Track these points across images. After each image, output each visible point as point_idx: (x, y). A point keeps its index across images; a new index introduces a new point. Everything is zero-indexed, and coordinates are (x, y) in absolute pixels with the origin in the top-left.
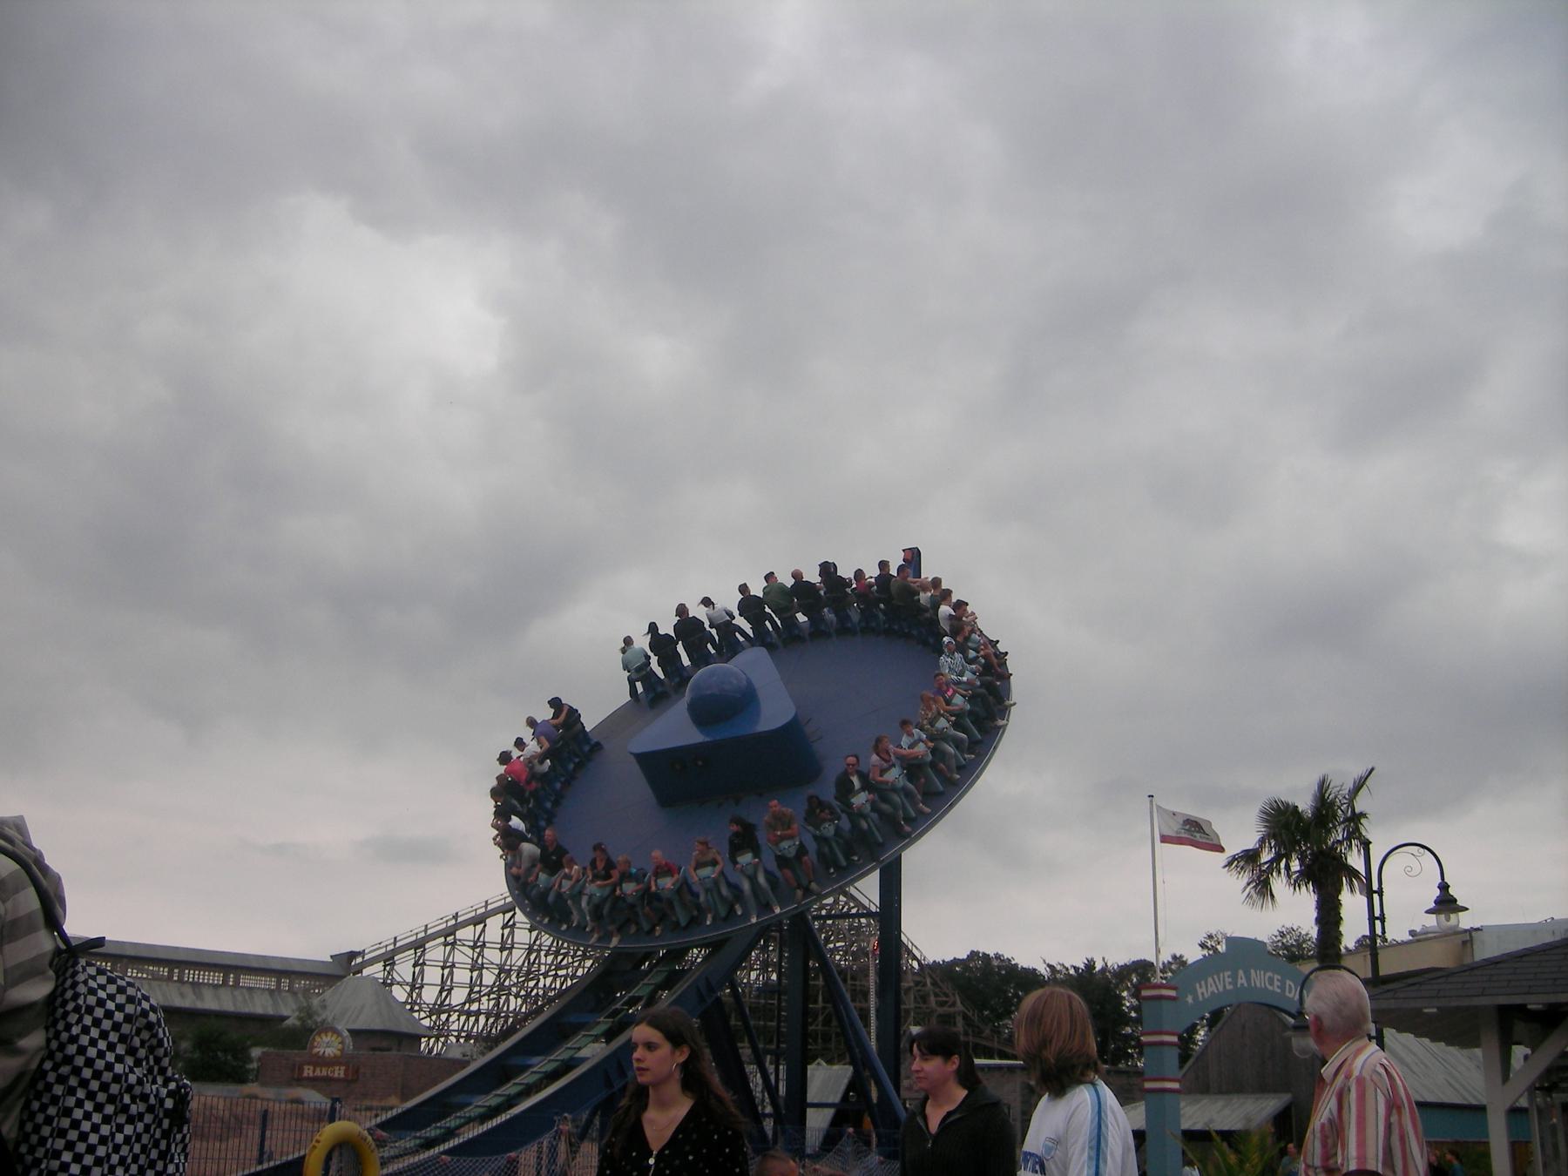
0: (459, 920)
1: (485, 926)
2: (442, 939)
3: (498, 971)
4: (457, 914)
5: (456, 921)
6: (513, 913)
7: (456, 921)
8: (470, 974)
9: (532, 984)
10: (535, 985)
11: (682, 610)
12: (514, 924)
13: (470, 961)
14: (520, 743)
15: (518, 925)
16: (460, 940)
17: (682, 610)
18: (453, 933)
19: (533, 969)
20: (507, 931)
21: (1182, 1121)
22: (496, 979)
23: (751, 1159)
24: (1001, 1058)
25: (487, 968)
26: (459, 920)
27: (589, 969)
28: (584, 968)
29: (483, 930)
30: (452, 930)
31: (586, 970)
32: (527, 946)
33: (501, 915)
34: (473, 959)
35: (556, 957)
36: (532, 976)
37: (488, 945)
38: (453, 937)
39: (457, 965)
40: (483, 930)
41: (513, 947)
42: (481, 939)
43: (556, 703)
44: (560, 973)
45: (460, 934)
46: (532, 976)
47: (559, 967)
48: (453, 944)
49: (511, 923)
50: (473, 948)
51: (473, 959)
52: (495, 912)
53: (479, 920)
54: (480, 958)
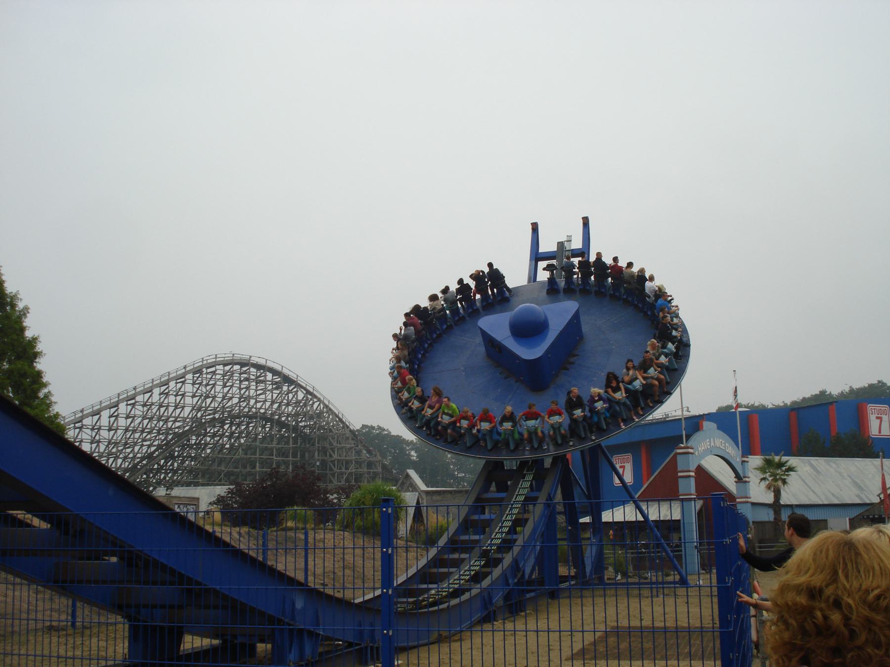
0: (85, 413)
1: (100, 416)
2: (73, 425)
3: (107, 443)
4: (83, 409)
5: (185, 370)
6: (167, 386)
7: (185, 370)
8: (90, 446)
9: (128, 450)
10: (131, 451)
11: (461, 282)
12: (118, 415)
13: (90, 438)
14: (39, 349)
15: (120, 415)
16: (85, 425)
17: (461, 282)
18: (81, 421)
19: (129, 442)
20: (112, 419)
21: (703, 460)
22: (106, 448)
23: (379, 580)
24: (609, 550)
25: (105, 439)
26: (85, 413)
27: (145, 455)
28: (223, 393)
29: (99, 419)
30: (116, 404)
31: (143, 454)
32: (124, 428)
33: (142, 395)
34: (91, 436)
35: (142, 434)
36: (128, 446)
37: (102, 428)
38: (81, 423)
39: (84, 441)
40: (99, 419)
41: (117, 429)
42: (98, 424)
43: (490, 265)
44: (145, 443)
45: (86, 421)
46: (128, 446)
47: (144, 440)
48: (81, 428)
49: (116, 414)
50: (93, 429)
51: (91, 436)
52: (105, 408)
53: (98, 413)
54: (98, 435)
